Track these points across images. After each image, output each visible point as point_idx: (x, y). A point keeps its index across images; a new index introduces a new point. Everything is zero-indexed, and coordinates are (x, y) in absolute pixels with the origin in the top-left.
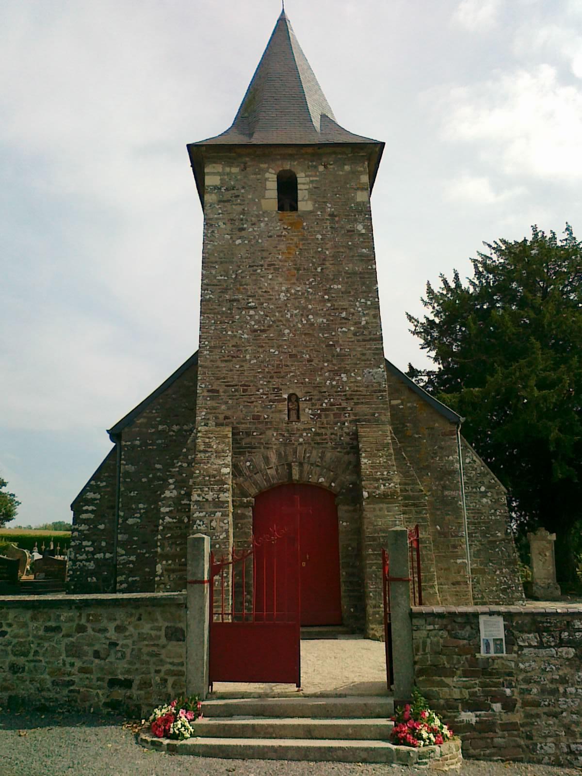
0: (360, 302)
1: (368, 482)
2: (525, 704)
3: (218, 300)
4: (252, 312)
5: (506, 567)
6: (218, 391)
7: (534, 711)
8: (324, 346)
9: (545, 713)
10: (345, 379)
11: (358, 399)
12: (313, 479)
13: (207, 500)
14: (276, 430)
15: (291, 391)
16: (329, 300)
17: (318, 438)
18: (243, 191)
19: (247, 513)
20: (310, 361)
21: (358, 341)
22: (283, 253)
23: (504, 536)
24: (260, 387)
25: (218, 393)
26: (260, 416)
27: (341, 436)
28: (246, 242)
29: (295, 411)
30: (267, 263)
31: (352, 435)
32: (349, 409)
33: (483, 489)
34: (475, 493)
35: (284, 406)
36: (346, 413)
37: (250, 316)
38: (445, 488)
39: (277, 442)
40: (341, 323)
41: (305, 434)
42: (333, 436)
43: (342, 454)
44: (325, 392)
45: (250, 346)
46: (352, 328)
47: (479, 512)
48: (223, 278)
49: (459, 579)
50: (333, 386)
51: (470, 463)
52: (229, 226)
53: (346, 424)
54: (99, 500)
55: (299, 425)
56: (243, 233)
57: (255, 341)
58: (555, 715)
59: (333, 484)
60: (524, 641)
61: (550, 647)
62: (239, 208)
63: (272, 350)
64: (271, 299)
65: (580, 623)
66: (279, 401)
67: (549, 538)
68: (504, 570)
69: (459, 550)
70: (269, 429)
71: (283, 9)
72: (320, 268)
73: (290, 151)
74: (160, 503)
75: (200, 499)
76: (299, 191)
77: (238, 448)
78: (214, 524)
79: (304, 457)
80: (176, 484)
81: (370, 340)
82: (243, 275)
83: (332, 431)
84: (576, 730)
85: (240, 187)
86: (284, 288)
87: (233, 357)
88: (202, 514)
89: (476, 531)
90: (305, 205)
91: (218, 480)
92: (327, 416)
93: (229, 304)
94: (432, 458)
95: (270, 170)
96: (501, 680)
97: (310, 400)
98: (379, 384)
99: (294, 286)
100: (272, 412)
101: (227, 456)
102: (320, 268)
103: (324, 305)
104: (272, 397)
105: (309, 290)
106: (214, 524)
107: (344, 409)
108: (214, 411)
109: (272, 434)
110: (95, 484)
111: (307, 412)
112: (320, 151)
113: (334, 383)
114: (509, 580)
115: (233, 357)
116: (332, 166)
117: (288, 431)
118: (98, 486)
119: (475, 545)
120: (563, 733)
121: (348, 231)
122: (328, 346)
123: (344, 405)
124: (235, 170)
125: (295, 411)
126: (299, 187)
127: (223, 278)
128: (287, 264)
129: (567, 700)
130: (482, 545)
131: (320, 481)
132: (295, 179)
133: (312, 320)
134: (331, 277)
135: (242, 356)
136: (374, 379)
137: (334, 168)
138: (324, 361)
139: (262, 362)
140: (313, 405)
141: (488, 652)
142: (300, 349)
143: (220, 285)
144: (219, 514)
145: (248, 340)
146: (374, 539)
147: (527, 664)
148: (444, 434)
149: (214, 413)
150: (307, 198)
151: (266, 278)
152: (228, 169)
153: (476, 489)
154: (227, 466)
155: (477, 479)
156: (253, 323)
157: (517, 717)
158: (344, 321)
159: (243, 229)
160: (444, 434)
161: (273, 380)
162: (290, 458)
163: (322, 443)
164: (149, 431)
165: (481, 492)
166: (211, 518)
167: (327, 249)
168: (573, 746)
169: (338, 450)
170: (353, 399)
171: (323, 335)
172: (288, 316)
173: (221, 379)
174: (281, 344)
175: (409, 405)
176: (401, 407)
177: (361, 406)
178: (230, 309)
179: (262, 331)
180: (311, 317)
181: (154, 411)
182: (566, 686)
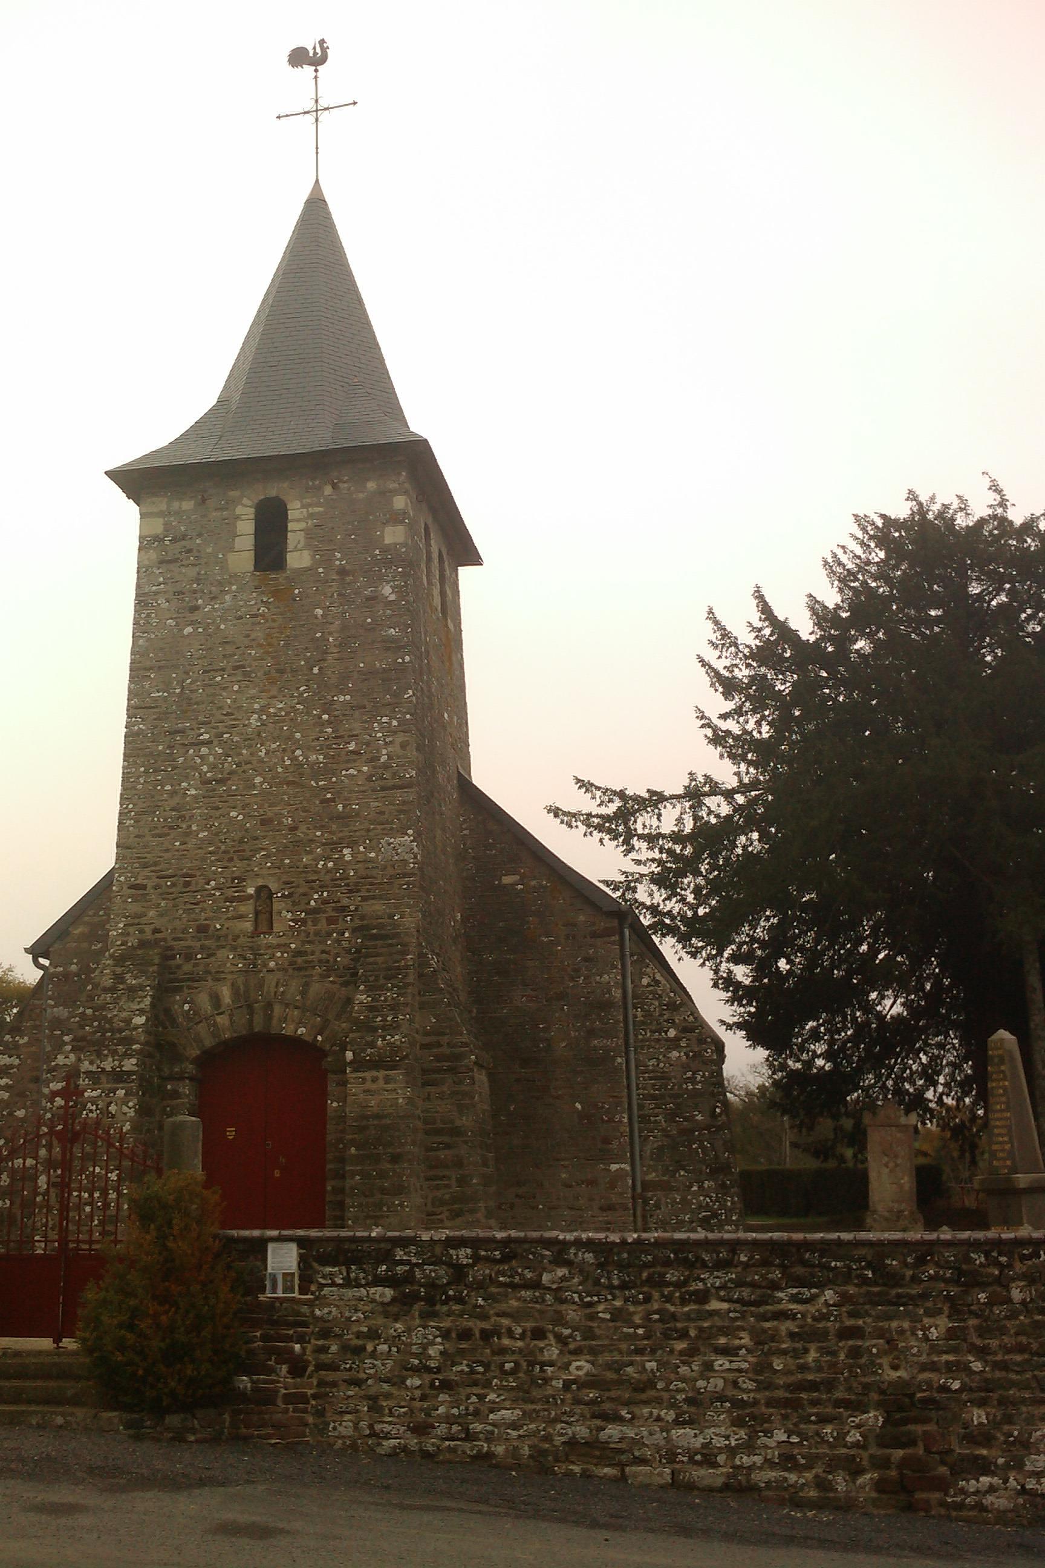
0: (380, 723)
1: (358, 1034)
3: (152, 733)
4: (204, 750)
6: (144, 887)
7: (330, 1376)
8: (318, 802)
9: (345, 1381)
10: (348, 858)
11: (368, 891)
12: (288, 1029)
13: (103, 1070)
14: (234, 949)
15: (260, 882)
16: (329, 722)
17: (300, 960)
19: (181, 1090)
20: (293, 829)
21: (374, 790)
22: (261, 645)
24: (211, 876)
25: (145, 890)
26: (208, 926)
28: (200, 630)
29: (264, 918)
31: (355, 953)
32: (352, 908)
33: (672, 1033)
34: (658, 1040)
35: (248, 908)
36: (346, 916)
37: (201, 757)
38: (591, 1033)
39: (234, 969)
40: (348, 761)
41: (279, 954)
42: (324, 956)
43: (337, 986)
44: (314, 881)
45: (198, 808)
46: (365, 769)
47: (664, 1077)
48: (161, 694)
49: (614, 1199)
50: (329, 871)
51: (649, 985)
54: (18, 1067)
55: (271, 939)
56: (197, 616)
57: (206, 800)
58: (357, 1383)
59: (319, 1038)
60: (324, 1277)
61: (359, 1286)
62: (192, 572)
63: (233, 814)
64: (234, 726)
65: (402, 1253)
66: (240, 900)
67: (903, 1120)
68: (706, 1184)
70: (223, 947)
71: (317, 181)
72: (317, 668)
75: (93, 1068)
76: (289, 534)
78: (113, 1108)
79: (276, 993)
80: (74, 1043)
82: (194, 687)
83: (322, 947)
84: (385, 1404)
87: (171, 828)
88: (95, 1094)
89: (657, 1110)
90: (298, 559)
91: (125, 1038)
92: (315, 922)
93: (168, 738)
94: (572, 979)
95: (245, 501)
96: (291, 1332)
97: (291, 895)
98: (405, 862)
99: (274, 701)
100: (228, 919)
101: (145, 997)
102: (317, 668)
103: (321, 732)
104: (230, 893)
105: (298, 706)
106: (113, 1108)
108: (136, 921)
110: (11, 1040)
113: (330, 864)
114: (714, 1202)
115: (171, 828)
116: (346, 485)
117: (251, 948)
118: (16, 1046)
119: (654, 1137)
120: (366, 1409)
121: (368, 599)
123: (345, 902)
124: (188, 505)
125: (264, 918)
126: (291, 526)
127: (161, 694)
129: (376, 1362)
130: (667, 1136)
131: (299, 1032)
133: (301, 758)
135: (184, 826)
136: (397, 854)
137: (349, 489)
138: (316, 828)
139: (217, 834)
140: (294, 904)
143: (157, 707)
144: (121, 1093)
147: (326, 1310)
148: (594, 935)
149: (138, 924)
150: (302, 543)
151: (229, 689)
152: (176, 505)
153: (660, 1034)
154: (142, 1012)
155: (661, 1015)
156: (205, 768)
159: (196, 608)
160: (594, 935)
161: (232, 864)
163: (306, 969)
164: (93, 947)
165: (668, 1040)
166: (109, 1100)
167: (330, 633)
169: (331, 979)
170: (358, 891)
171: (317, 784)
172: (262, 754)
173: (151, 866)
174: (247, 801)
175: (533, 883)
176: (520, 887)
177: (373, 901)
178: (171, 747)
179: (220, 782)
181: (101, 913)
182: (377, 1342)
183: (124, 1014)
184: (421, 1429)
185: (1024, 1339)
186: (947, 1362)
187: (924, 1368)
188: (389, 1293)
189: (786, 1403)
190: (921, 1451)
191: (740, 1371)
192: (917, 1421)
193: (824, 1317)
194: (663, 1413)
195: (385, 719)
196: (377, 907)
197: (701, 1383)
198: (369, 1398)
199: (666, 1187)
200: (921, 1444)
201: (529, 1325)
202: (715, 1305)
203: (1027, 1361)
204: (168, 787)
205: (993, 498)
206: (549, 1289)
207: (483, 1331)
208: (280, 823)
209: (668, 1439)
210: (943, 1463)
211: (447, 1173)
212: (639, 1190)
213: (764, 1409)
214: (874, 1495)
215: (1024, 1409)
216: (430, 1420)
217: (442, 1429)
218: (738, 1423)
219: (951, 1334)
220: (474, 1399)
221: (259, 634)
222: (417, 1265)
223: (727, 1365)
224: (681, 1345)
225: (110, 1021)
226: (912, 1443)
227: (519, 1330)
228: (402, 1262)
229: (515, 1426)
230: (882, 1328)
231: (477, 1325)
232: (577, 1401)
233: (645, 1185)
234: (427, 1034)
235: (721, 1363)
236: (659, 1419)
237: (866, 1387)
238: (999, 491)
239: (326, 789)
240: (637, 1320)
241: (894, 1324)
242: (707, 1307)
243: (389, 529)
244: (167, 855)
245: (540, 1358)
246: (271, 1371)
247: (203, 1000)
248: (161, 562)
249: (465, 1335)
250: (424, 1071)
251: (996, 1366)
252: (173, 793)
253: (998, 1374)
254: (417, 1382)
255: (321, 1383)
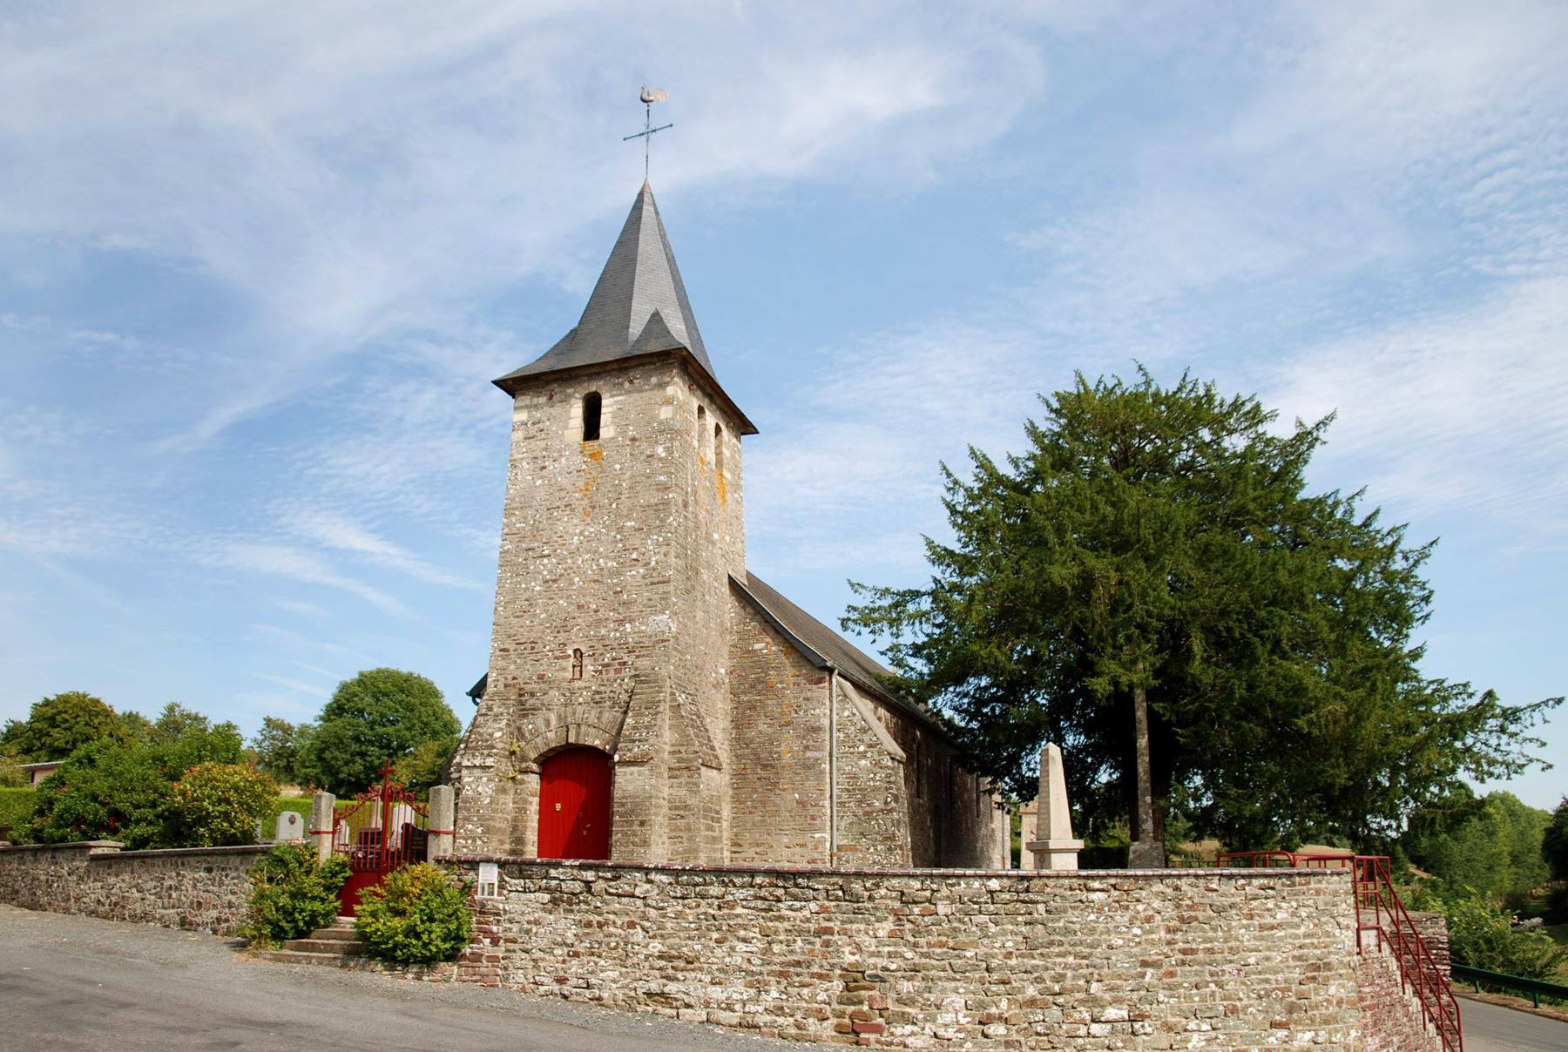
2: (506, 941)
4: (545, 561)
5: (882, 842)
7: (511, 946)
10: (629, 630)
14: (559, 689)
15: (576, 647)
17: (597, 697)
18: (548, 423)
20: (596, 611)
22: (581, 490)
23: (883, 806)
26: (544, 675)
27: (620, 693)
30: (564, 503)
33: (862, 748)
34: (851, 753)
37: (544, 565)
40: (631, 566)
42: (612, 695)
46: (641, 571)
47: (855, 777)
49: (816, 856)
52: (532, 467)
53: (626, 680)
56: (544, 472)
58: (526, 951)
62: (542, 444)
63: (561, 602)
64: (564, 545)
66: (563, 658)
68: (879, 848)
69: (818, 821)
73: (595, 370)
74: (1198, 780)
77: (522, 710)
81: (659, 582)
85: (545, 419)
86: (578, 531)
90: (607, 430)
95: (577, 395)
97: (594, 654)
99: (588, 527)
104: (557, 653)
106: (480, 789)
107: (625, 663)
109: (554, 693)
111: (589, 668)
112: (625, 365)
113: (618, 635)
121: (648, 457)
122: (616, 593)
123: (626, 659)
126: (603, 410)
128: (583, 502)
132: (599, 399)
134: (625, 512)
141: (483, 894)
142: (587, 599)
144: (485, 779)
145: (539, 592)
146: (623, 805)
152: (535, 400)
154: (501, 729)
156: (545, 573)
157: (500, 951)
158: (634, 563)
162: (569, 720)
168: (537, 978)
172: (580, 562)
176: (765, 651)
178: (525, 560)
179: (555, 581)
180: (601, 561)
183: (490, 731)
184: (561, 981)
185: (944, 939)
186: (889, 952)
187: (872, 954)
188: (547, 897)
189: (781, 974)
190: (866, 1008)
191: (752, 953)
192: (864, 988)
193: (808, 920)
194: (703, 977)
195: (655, 537)
196: (645, 662)
197: (727, 960)
198: (534, 960)
199: (853, 849)
200: (866, 1003)
201: (627, 919)
202: (739, 910)
203: (945, 953)
204: (523, 586)
205: (1140, 379)
206: (639, 897)
207: (598, 922)
208: (589, 608)
209: (705, 994)
210: (881, 1016)
211: (681, 834)
212: (835, 851)
213: (766, 977)
214: (835, 1034)
215: (940, 983)
216: (566, 975)
217: (573, 981)
218: (750, 985)
219: (892, 935)
220: (592, 964)
221: (581, 484)
222: (563, 880)
223: (745, 949)
224: (715, 935)
225: (481, 734)
226: (861, 1002)
227: (620, 923)
228: (555, 878)
229: (614, 981)
230: (846, 929)
231: (595, 918)
232: (652, 968)
233: (840, 848)
234: (673, 745)
235: (741, 946)
236: (700, 981)
237: (833, 966)
238: (1145, 374)
239: (616, 585)
240: (691, 918)
241: (855, 926)
242: (734, 912)
243: (664, 409)
244: (521, 630)
245: (631, 940)
246: (480, 942)
247: (540, 722)
248: (525, 439)
249: (589, 924)
250: (670, 769)
251: (923, 955)
252: (527, 589)
253: (923, 960)
254: (560, 952)
255: (508, 951)
